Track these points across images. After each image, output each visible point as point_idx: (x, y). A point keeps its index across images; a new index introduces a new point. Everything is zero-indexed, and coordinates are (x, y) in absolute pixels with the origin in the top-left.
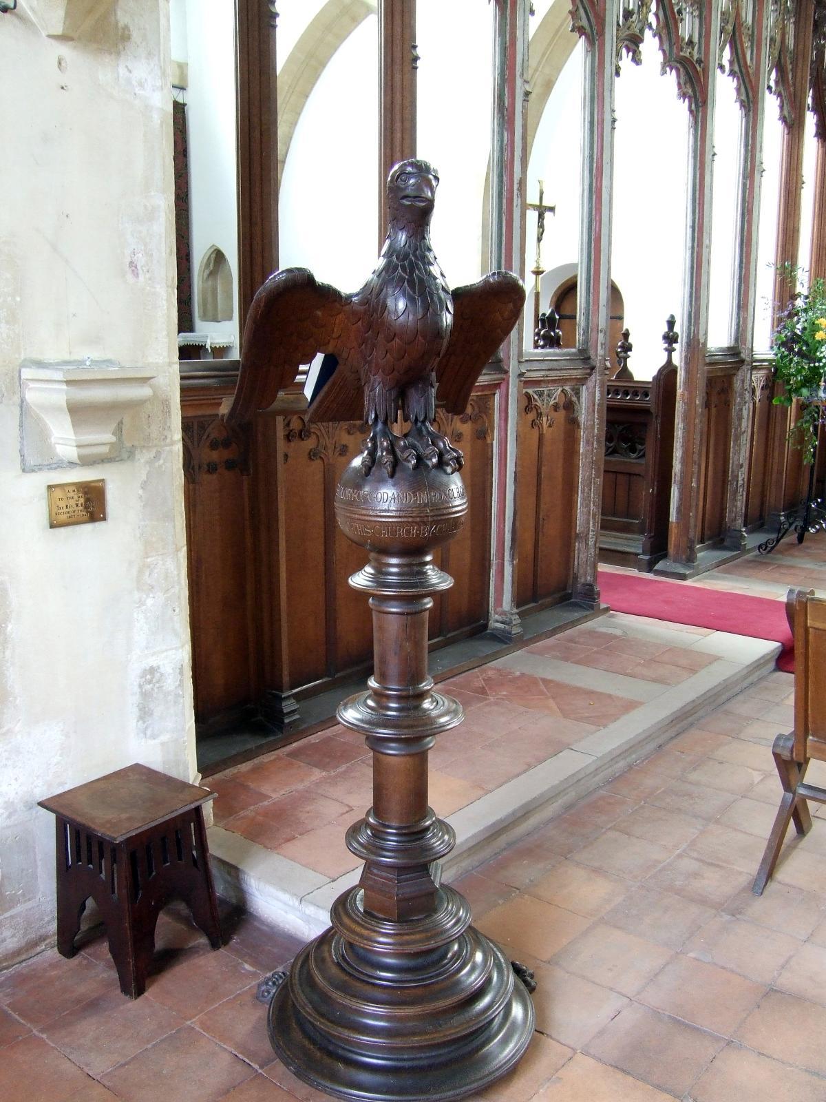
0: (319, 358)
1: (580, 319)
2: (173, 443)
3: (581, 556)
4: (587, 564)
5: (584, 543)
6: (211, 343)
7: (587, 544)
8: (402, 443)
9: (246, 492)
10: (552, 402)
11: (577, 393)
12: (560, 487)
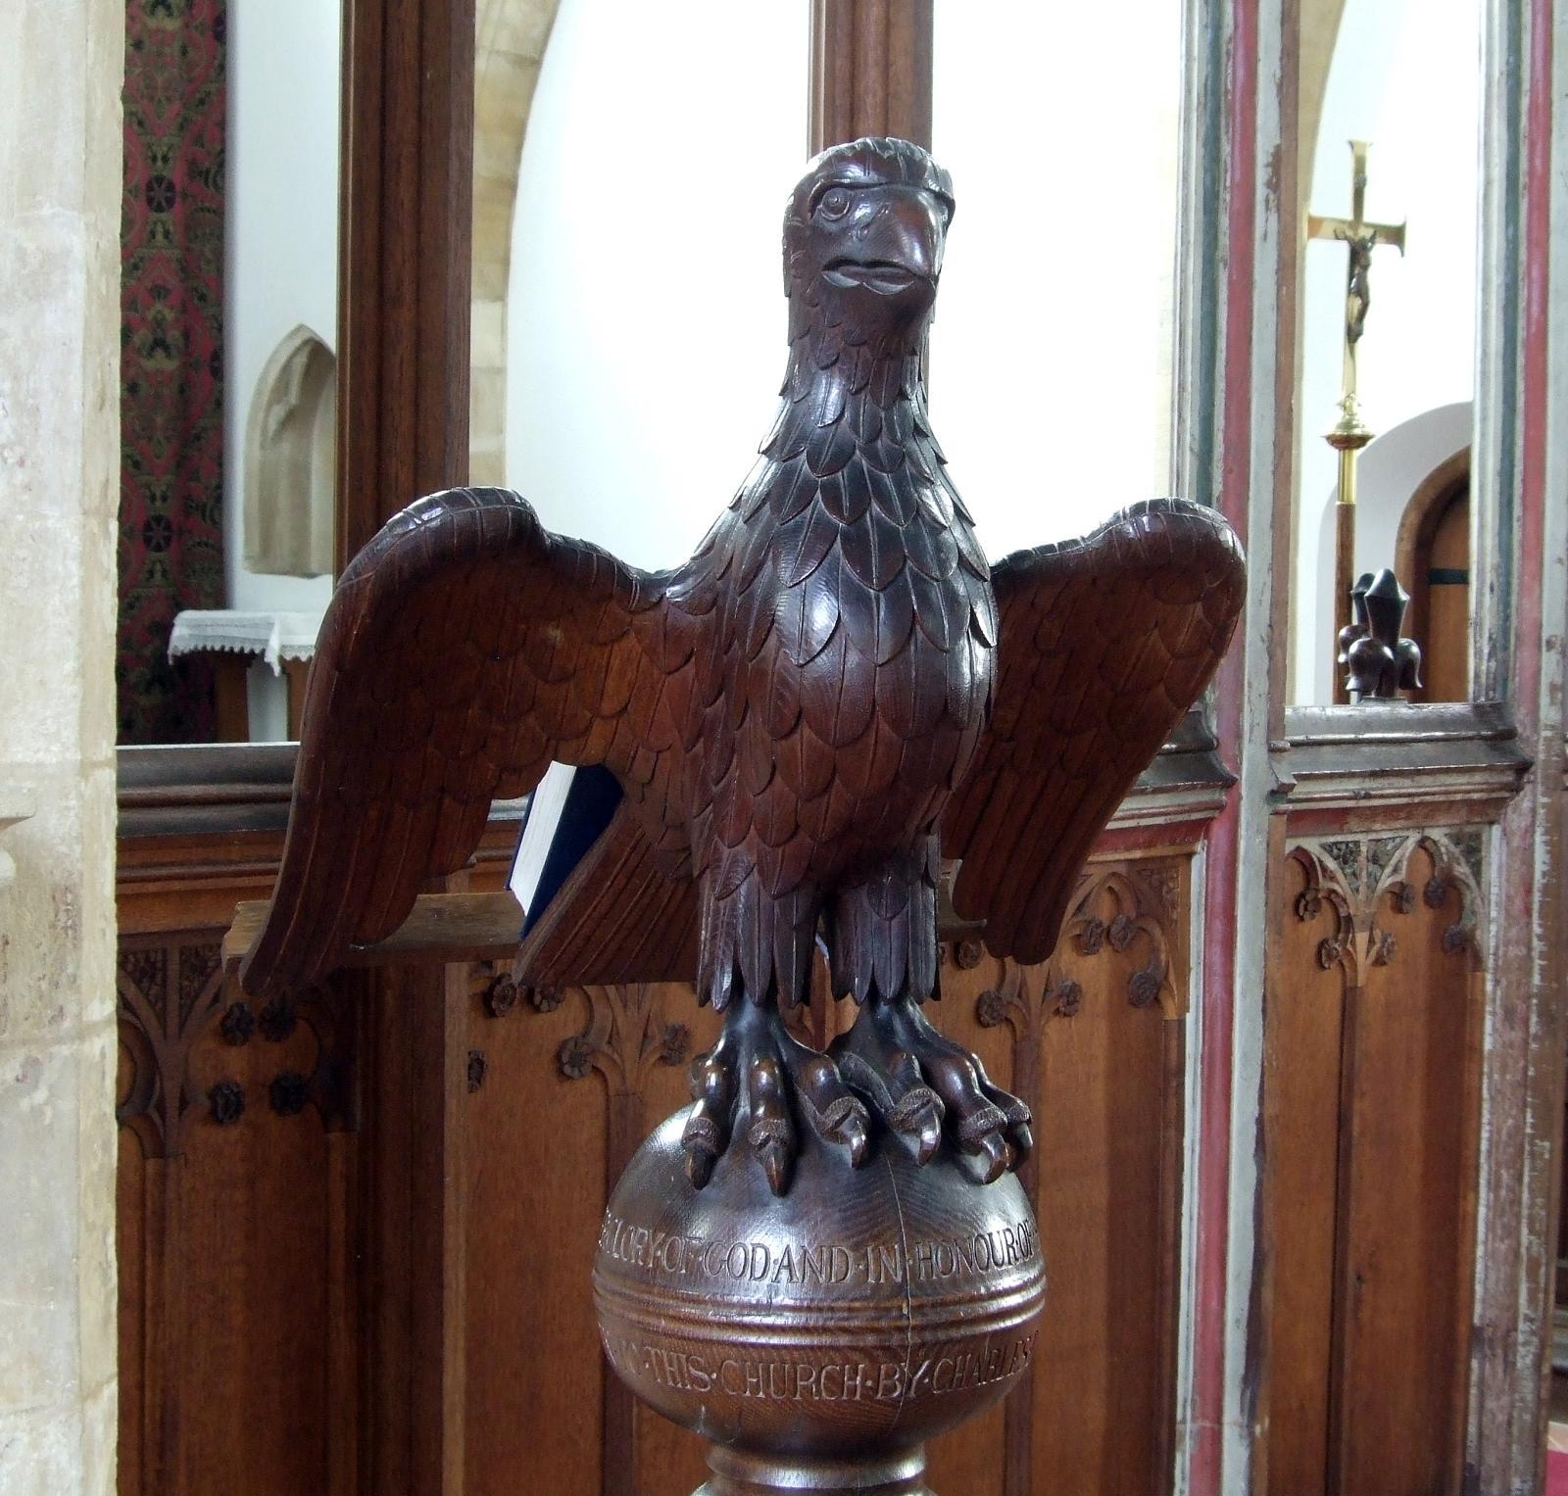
0: (557, 781)
1: (1480, 604)
2: (83, 1033)
3: (1491, 1404)
4: (1510, 1433)
5: (1499, 1361)
6: (283, 647)
7: (1509, 1365)
8: (821, 1076)
9: (338, 1189)
10: (1386, 881)
11: (1473, 851)
12: (1415, 1168)
